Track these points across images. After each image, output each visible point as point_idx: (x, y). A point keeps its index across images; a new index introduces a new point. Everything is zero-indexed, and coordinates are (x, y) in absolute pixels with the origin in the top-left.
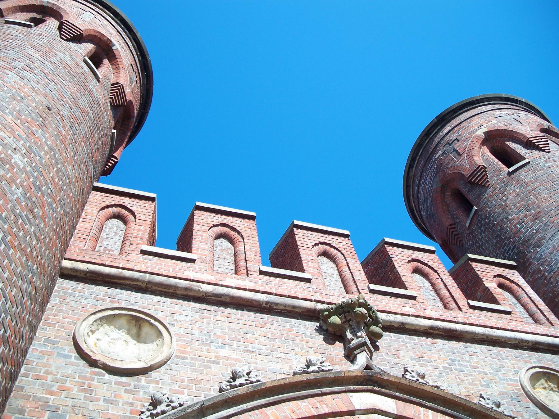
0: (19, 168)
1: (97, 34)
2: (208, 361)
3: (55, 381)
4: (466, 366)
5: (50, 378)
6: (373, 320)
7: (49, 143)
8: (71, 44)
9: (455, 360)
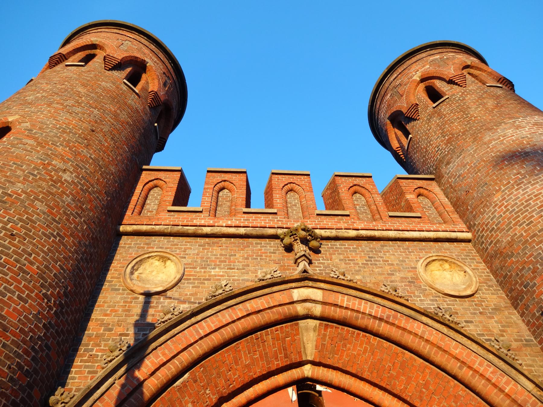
0: (68, 182)
1: (132, 58)
2: (204, 280)
3: (109, 307)
4: (379, 261)
5: (106, 305)
6: (312, 237)
7: (93, 157)
8: (113, 72)
9: (372, 257)
